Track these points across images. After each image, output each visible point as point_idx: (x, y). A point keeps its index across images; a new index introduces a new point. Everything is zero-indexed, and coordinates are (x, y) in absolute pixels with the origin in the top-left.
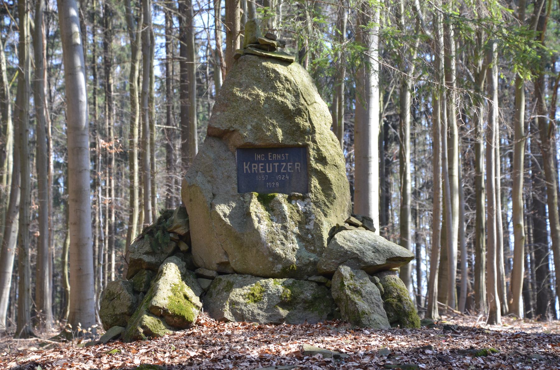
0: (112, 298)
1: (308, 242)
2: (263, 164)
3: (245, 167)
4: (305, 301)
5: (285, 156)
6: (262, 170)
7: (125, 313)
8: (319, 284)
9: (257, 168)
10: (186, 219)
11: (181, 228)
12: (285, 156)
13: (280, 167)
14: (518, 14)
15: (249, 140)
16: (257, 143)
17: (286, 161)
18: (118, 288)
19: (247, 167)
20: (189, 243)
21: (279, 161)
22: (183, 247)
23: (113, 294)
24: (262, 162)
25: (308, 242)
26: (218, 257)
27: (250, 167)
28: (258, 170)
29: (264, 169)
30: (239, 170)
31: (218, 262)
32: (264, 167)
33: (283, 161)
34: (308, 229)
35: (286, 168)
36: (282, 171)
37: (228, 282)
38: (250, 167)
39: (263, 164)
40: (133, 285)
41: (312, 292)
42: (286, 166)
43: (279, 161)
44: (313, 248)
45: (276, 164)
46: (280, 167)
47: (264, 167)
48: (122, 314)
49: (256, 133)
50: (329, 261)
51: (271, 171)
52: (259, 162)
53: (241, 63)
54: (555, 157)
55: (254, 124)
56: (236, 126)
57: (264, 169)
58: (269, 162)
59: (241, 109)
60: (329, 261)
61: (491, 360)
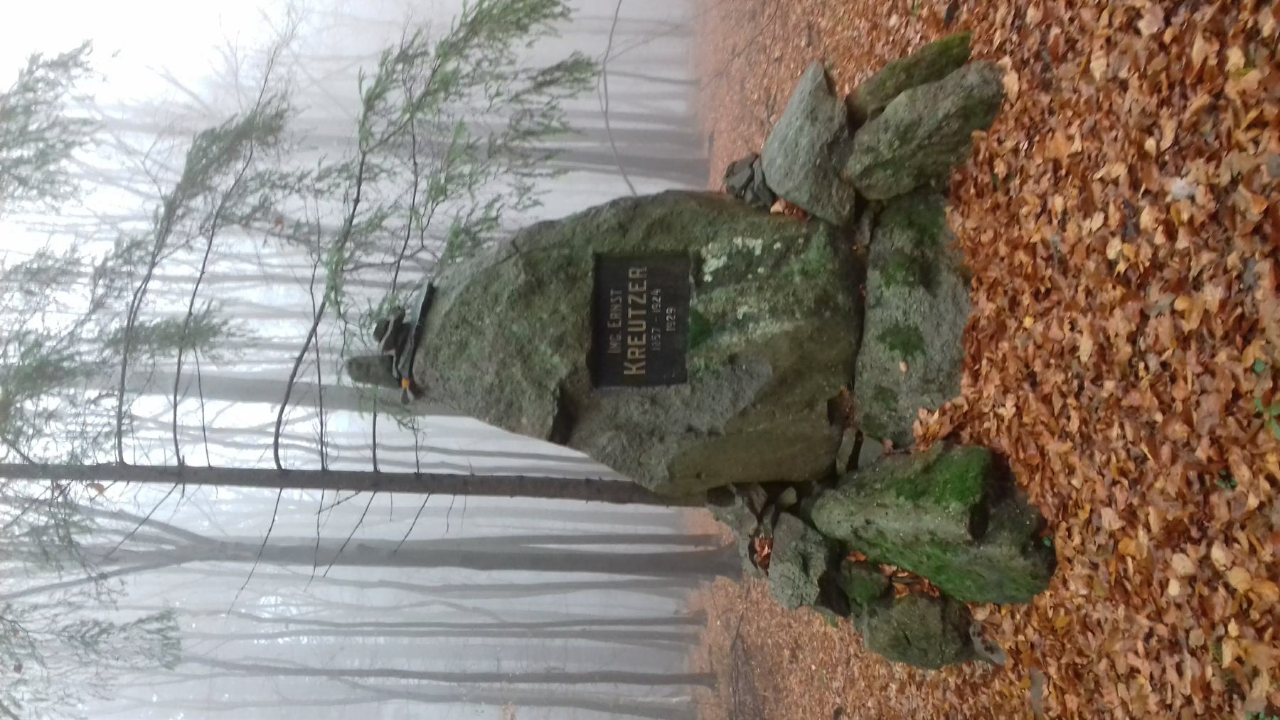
0: (905, 641)
1: (788, 249)
2: (629, 339)
3: (634, 372)
4: (918, 244)
5: (615, 296)
6: (640, 339)
7: (943, 611)
8: (876, 224)
9: (635, 348)
10: (734, 490)
11: (754, 497)
12: (615, 296)
13: (635, 306)
14: (172, 634)
15: (582, 359)
16: (587, 345)
17: (626, 294)
18: (886, 627)
19: (634, 368)
20: (782, 485)
21: (625, 306)
22: (790, 496)
23: (896, 638)
24: (624, 341)
25: (788, 249)
26: (817, 424)
27: (634, 361)
28: (640, 347)
29: (639, 335)
30: (637, 381)
31: (824, 422)
32: (634, 335)
33: (625, 300)
34: (763, 250)
35: (640, 295)
36: (644, 301)
37: (875, 398)
38: (634, 361)
39: (629, 339)
40: (873, 599)
41: (896, 231)
42: (636, 294)
43: (625, 306)
44: (801, 241)
45: (630, 312)
46: (635, 306)
47: (634, 335)
48: (943, 618)
49: (568, 347)
50: (835, 199)
51: (644, 323)
52: (624, 345)
53: (427, 379)
54: (574, 169)
55: (549, 352)
56: (553, 385)
57: (639, 335)
58: (625, 325)
59: (519, 376)
60: (835, 199)
61: (901, 690)
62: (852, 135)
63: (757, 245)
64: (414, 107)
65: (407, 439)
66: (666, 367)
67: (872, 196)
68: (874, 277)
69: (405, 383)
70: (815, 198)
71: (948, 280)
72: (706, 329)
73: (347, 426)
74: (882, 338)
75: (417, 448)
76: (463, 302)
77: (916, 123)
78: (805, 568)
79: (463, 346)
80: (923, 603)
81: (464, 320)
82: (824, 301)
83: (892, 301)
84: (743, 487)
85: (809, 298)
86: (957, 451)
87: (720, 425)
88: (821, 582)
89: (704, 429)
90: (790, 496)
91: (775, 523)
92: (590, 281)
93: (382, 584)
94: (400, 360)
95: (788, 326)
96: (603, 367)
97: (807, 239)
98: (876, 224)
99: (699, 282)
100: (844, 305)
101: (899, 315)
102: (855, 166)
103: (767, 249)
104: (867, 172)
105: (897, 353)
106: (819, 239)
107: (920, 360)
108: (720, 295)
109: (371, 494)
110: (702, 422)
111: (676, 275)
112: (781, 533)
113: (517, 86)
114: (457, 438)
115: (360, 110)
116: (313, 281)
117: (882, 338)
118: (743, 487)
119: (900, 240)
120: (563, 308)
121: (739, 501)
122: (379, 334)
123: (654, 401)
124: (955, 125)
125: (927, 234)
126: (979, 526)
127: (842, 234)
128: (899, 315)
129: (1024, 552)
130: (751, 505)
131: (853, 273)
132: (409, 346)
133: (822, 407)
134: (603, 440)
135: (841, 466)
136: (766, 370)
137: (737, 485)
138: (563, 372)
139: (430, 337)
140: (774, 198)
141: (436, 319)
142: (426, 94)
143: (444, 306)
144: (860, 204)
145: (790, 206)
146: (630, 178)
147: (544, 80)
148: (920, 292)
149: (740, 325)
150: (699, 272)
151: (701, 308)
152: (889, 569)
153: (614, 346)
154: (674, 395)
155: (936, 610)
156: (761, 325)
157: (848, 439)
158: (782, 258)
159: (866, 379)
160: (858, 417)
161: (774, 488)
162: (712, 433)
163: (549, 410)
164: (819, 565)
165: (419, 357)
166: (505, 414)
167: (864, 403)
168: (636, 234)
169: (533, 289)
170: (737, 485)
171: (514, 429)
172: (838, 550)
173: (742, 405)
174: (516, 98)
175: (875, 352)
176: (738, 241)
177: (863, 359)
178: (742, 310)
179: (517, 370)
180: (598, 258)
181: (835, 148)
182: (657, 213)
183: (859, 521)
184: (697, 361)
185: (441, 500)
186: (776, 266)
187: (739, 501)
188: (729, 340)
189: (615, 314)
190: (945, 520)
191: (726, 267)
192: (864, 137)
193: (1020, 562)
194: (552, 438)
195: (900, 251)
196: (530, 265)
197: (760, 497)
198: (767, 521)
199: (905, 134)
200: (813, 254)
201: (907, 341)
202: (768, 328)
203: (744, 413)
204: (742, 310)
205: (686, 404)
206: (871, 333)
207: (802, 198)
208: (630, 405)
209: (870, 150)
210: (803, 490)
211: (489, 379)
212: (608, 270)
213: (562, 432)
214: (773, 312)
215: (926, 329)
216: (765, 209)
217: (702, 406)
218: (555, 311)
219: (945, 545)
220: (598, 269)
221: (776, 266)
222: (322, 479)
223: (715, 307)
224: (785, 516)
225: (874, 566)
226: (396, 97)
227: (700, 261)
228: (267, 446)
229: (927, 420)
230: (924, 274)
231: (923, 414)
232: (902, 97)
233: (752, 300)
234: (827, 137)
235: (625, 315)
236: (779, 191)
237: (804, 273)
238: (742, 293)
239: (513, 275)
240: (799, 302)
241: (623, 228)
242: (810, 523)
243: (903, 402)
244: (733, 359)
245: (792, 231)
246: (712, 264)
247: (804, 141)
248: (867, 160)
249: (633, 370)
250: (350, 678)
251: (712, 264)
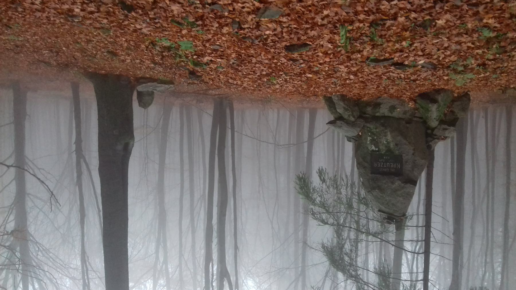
8: (365, 113)
13: (383, 165)
15: (396, 178)
16: (393, 176)
29: (390, 165)
46: (383, 165)
52: (393, 168)
56: (403, 185)
57: (390, 165)
62: (345, 119)
63: (369, 138)
64: (328, 212)
65: (415, 217)
66: (398, 159)
67: (359, 114)
68: (377, 114)
69: (402, 218)
70: (359, 127)
71: (379, 100)
72: (389, 150)
73: (409, 234)
74: (392, 113)
75: (418, 215)
76: (383, 204)
77: (344, 108)
78: (446, 129)
79: (393, 204)
80: (453, 106)
81: (387, 204)
82: (383, 125)
83: (384, 111)
84: (427, 142)
85: (382, 128)
86: (418, 101)
87: (412, 148)
88: (449, 126)
89: (413, 152)
90: (429, 131)
91: (436, 135)
92: (377, 175)
93: (472, 228)
94: (396, 218)
95: (389, 133)
96: (398, 174)
97: (368, 127)
98: (365, 113)
99: (378, 151)
100: (385, 121)
101: (386, 110)
102: (353, 119)
103: (370, 136)
104: (354, 117)
105: (395, 110)
106: (368, 125)
107: (397, 106)
108: (381, 147)
109: (432, 229)
110: (412, 152)
111: (376, 156)
112: (438, 134)
113: (324, 186)
114: (415, 205)
115: (327, 226)
116: (367, 241)
117: (392, 113)
118: (427, 142)
119: (369, 109)
120: (384, 182)
121: (430, 143)
122: (390, 223)
123: (406, 162)
124: (346, 102)
125: (368, 104)
126: (434, 101)
127: (367, 120)
128: (386, 110)
129: (440, 94)
130: (431, 141)
131: (375, 119)
132: (393, 217)
133: (408, 125)
134: (416, 174)
135: (422, 120)
136: (399, 138)
137: (426, 143)
138: (400, 182)
139: (391, 211)
140: (359, 134)
141: (387, 210)
142: (324, 208)
143: (383, 208)
144: (360, 117)
145: (360, 131)
146: (315, 136)
147: (323, 181)
148: (381, 106)
149: (388, 143)
150: (376, 151)
151: (384, 151)
152: (446, 112)
153: (393, 170)
154: (405, 157)
155: (456, 103)
156: (388, 139)
157: (415, 119)
158: (373, 133)
159: (401, 116)
160: (410, 117)
161: (427, 135)
162: (414, 150)
163: (408, 185)
164: (446, 126)
165: (396, 214)
166: (410, 195)
167: (408, 116)
168: (366, 164)
169: (381, 189)
170: (426, 143)
171: (413, 194)
172: (442, 122)
173: (407, 143)
174: (328, 187)
175: (395, 114)
176: (368, 142)
177: (396, 116)
178: (385, 142)
179: (399, 193)
180: (371, 173)
181: (348, 123)
182: (361, 160)
183: (435, 120)
184: (397, 152)
185: (434, 209)
186: (374, 134)
187: (430, 143)
188: (392, 145)
189: (386, 170)
190: (434, 108)
191: (374, 145)
192: (346, 117)
193: (442, 95)
194: (415, 185)
195: (372, 109)
196: (374, 188)
197: (429, 139)
198: (435, 137)
199: (346, 110)
200: (372, 127)
201: (393, 108)
202: (389, 137)
203: (410, 143)
204: (385, 142)
205: (407, 155)
206: (390, 115)
207: (359, 129)
208: (408, 167)
209: (349, 116)
210: (428, 128)
211: (401, 199)
212: (375, 171)
213: (414, 183)
214: (385, 136)
215: (390, 105)
216: (360, 136)
217: (408, 152)
218: (385, 183)
219: (439, 106)
220: (374, 173)
221: (374, 134)
222: (427, 253)
223: (384, 148)
224: (434, 133)
225: (445, 115)
226: (324, 216)
227: (373, 150)
228: (418, 256)
229: (411, 104)
230: (377, 105)
231: (409, 106)
232: (338, 110)
233: (382, 140)
234: (345, 124)
235: (385, 168)
236: (357, 134)
237: (376, 129)
238: (381, 142)
239: (376, 192)
240: (383, 130)
241: (365, 167)
242: (436, 128)
243: (407, 109)
244: (396, 145)
245: (366, 131)
246: (373, 148)
247: (346, 129)
248: (351, 117)
249: (399, 166)
250: (511, 240)
251: (373, 148)
